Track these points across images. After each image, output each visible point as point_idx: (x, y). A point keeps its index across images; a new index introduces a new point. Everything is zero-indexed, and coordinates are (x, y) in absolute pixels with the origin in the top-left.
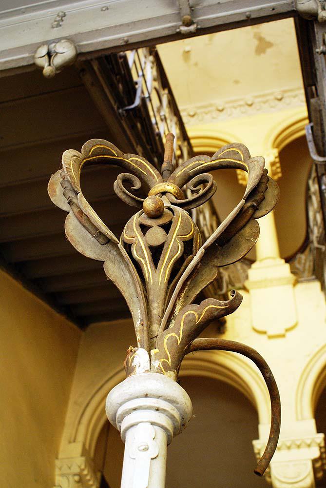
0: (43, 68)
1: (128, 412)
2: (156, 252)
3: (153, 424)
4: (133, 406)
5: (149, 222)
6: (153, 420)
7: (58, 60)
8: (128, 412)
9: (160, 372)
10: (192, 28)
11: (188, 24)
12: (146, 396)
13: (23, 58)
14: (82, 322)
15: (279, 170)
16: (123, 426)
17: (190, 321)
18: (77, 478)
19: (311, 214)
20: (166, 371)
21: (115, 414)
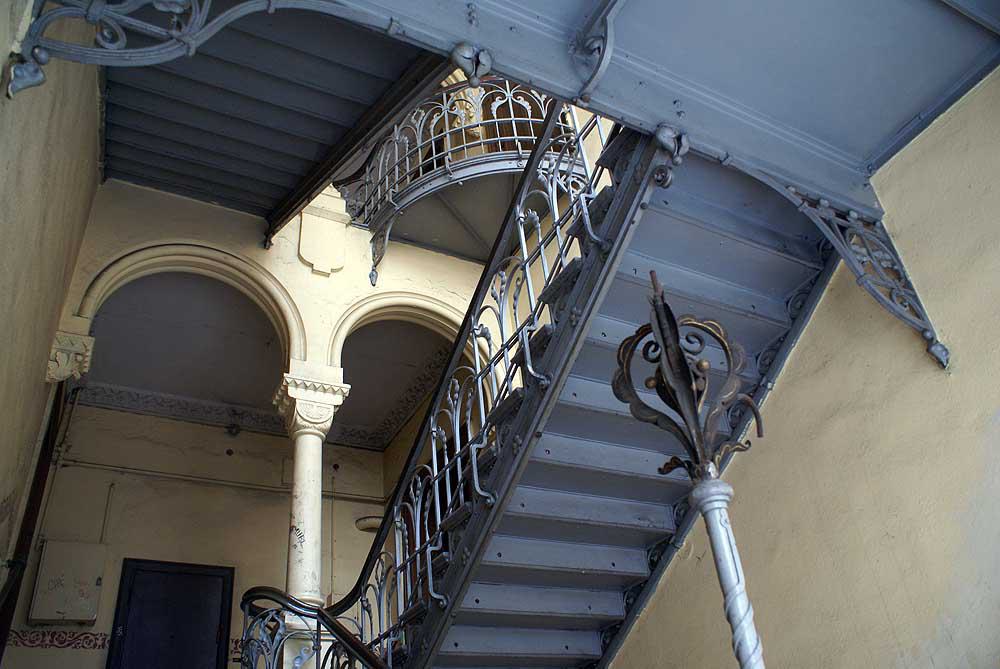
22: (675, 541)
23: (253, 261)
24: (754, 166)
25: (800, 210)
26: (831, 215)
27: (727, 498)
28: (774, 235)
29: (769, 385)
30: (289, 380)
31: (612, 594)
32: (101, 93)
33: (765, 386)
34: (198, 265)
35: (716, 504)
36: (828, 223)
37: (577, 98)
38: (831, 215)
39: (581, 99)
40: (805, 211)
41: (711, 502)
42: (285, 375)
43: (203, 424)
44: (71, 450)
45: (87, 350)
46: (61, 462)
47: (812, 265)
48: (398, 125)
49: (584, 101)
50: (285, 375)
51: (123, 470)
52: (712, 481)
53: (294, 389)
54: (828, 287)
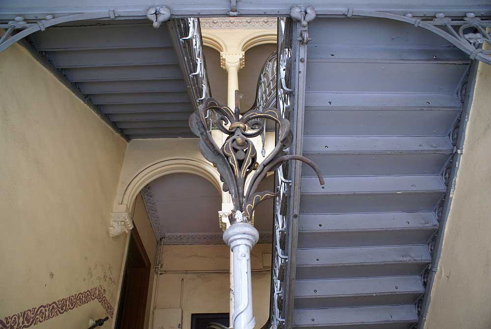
0: (152, 22)
1: (236, 240)
2: (241, 163)
3: (246, 245)
4: (239, 238)
5: (238, 148)
6: (247, 244)
7: (161, 18)
8: (236, 240)
9: (246, 222)
10: (235, 13)
11: (232, 11)
12: (244, 234)
13: (139, 11)
14: (128, 138)
15: (244, 63)
16: (232, 245)
17: (258, 200)
18: (123, 223)
19: (260, 93)
20: (249, 221)
21: (228, 240)
22: (432, 267)
23: (201, 160)
24: (373, 10)
25: (416, 25)
26: (449, 22)
27: (250, 237)
28: (419, 52)
29: (459, 152)
30: (221, 214)
31: (407, 306)
32: (83, 101)
33: (456, 153)
34: (174, 169)
35: (238, 242)
36: (444, 27)
37: (228, 12)
38: (449, 22)
39: (231, 11)
40: (420, 25)
41: (232, 241)
42: (219, 212)
43: (221, 244)
44: (164, 266)
45: (126, 219)
46: (160, 272)
47: (460, 62)
48: (262, 74)
49: (234, 12)
50: (219, 212)
51: (186, 272)
52: (237, 224)
53: (225, 218)
54: (478, 73)
